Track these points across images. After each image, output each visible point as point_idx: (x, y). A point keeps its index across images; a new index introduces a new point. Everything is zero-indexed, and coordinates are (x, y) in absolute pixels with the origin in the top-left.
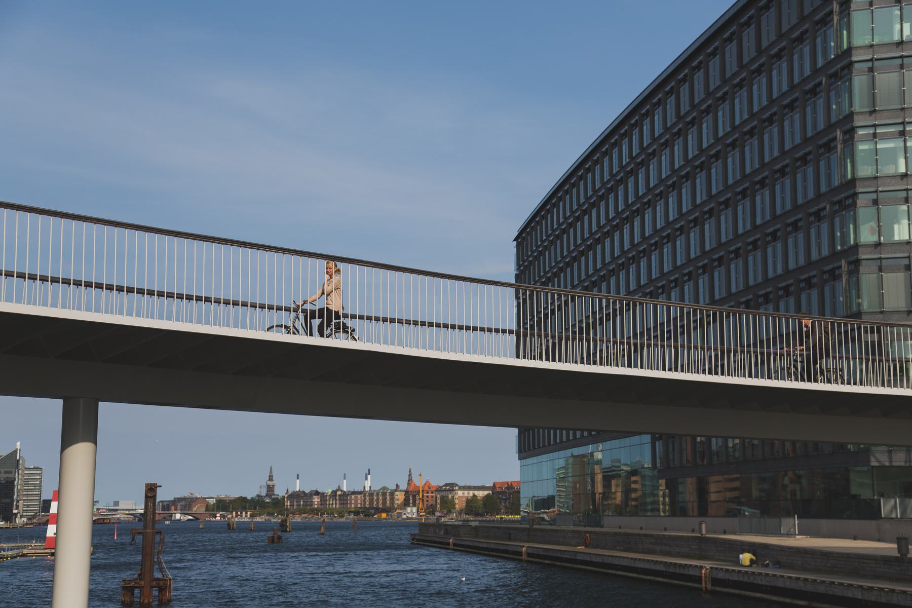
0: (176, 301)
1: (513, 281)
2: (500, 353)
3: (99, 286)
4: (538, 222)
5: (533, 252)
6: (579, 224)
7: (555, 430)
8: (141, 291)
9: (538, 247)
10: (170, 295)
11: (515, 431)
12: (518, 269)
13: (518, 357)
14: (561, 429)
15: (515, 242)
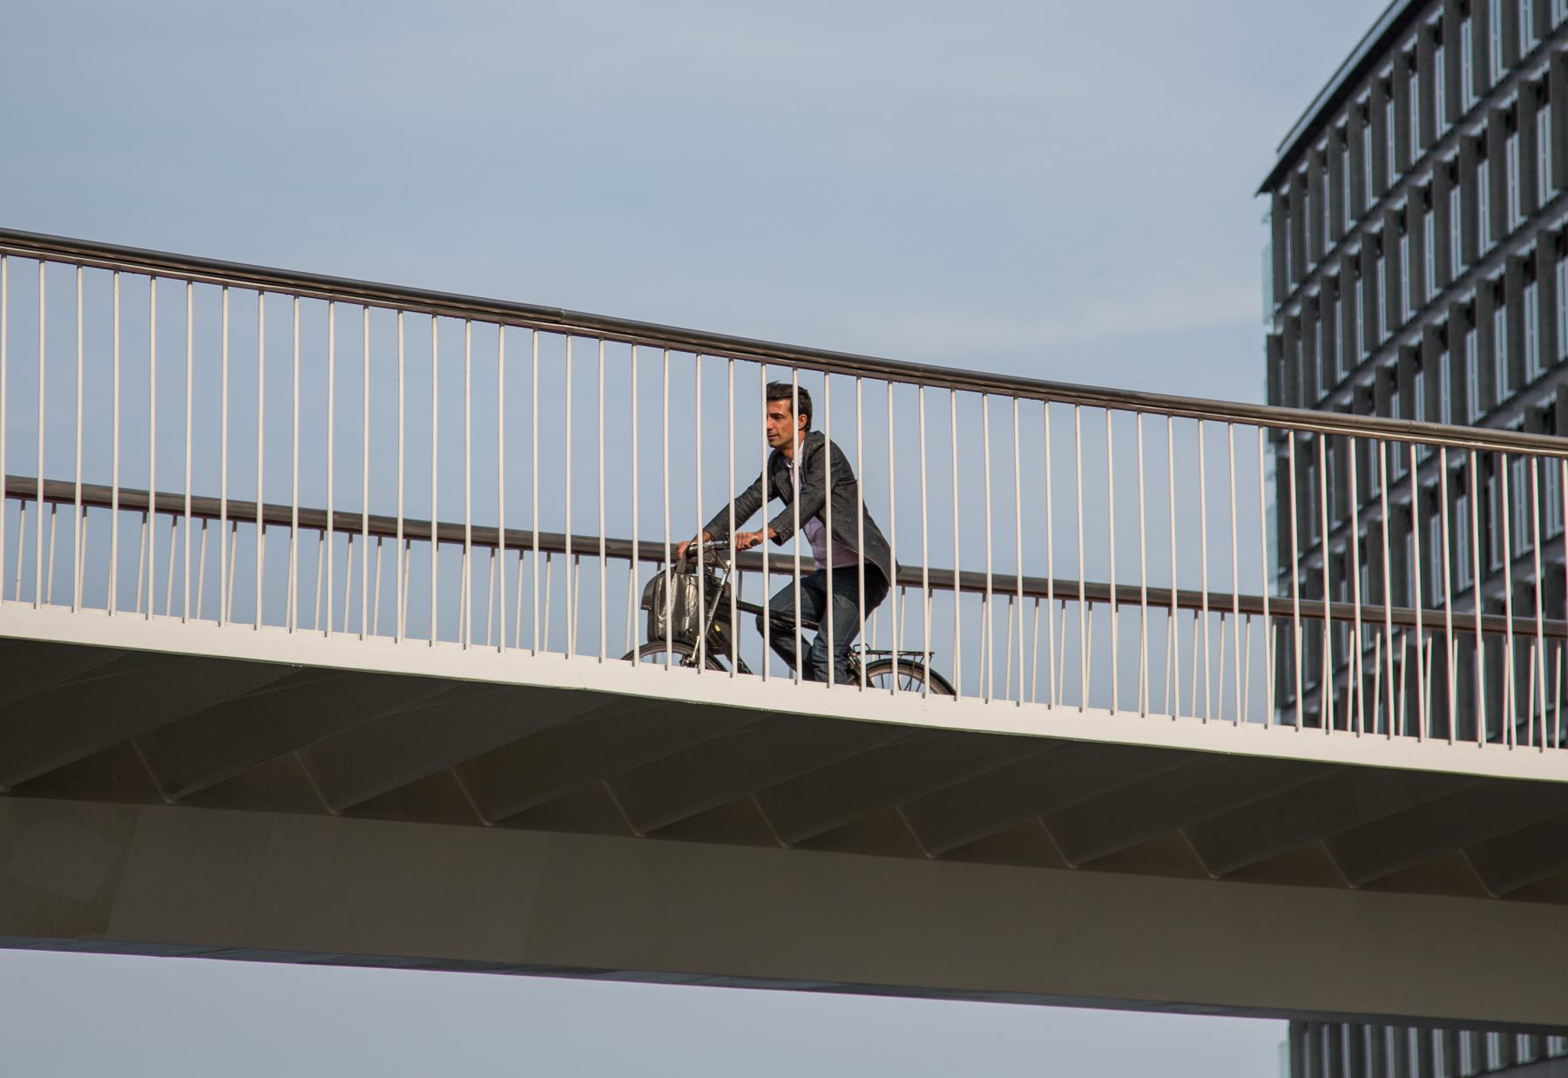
0: (473, 553)
1: (1257, 396)
2: (1212, 702)
3: (973, 584)
4: (1364, 112)
5: (1343, 240)
6: (1513, 144)
7: (1452, 1029)
8: (1159, 598)
9: (1364, 217)
10: (313, 520)
11: (1279, 1029)
12: (1279, 314)
13: (1285, 708)
14: (1480, 1028)
15: (1267, 199)
